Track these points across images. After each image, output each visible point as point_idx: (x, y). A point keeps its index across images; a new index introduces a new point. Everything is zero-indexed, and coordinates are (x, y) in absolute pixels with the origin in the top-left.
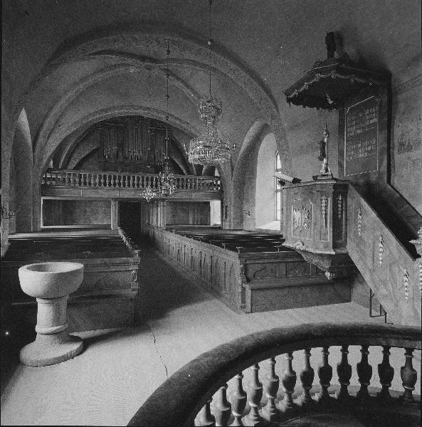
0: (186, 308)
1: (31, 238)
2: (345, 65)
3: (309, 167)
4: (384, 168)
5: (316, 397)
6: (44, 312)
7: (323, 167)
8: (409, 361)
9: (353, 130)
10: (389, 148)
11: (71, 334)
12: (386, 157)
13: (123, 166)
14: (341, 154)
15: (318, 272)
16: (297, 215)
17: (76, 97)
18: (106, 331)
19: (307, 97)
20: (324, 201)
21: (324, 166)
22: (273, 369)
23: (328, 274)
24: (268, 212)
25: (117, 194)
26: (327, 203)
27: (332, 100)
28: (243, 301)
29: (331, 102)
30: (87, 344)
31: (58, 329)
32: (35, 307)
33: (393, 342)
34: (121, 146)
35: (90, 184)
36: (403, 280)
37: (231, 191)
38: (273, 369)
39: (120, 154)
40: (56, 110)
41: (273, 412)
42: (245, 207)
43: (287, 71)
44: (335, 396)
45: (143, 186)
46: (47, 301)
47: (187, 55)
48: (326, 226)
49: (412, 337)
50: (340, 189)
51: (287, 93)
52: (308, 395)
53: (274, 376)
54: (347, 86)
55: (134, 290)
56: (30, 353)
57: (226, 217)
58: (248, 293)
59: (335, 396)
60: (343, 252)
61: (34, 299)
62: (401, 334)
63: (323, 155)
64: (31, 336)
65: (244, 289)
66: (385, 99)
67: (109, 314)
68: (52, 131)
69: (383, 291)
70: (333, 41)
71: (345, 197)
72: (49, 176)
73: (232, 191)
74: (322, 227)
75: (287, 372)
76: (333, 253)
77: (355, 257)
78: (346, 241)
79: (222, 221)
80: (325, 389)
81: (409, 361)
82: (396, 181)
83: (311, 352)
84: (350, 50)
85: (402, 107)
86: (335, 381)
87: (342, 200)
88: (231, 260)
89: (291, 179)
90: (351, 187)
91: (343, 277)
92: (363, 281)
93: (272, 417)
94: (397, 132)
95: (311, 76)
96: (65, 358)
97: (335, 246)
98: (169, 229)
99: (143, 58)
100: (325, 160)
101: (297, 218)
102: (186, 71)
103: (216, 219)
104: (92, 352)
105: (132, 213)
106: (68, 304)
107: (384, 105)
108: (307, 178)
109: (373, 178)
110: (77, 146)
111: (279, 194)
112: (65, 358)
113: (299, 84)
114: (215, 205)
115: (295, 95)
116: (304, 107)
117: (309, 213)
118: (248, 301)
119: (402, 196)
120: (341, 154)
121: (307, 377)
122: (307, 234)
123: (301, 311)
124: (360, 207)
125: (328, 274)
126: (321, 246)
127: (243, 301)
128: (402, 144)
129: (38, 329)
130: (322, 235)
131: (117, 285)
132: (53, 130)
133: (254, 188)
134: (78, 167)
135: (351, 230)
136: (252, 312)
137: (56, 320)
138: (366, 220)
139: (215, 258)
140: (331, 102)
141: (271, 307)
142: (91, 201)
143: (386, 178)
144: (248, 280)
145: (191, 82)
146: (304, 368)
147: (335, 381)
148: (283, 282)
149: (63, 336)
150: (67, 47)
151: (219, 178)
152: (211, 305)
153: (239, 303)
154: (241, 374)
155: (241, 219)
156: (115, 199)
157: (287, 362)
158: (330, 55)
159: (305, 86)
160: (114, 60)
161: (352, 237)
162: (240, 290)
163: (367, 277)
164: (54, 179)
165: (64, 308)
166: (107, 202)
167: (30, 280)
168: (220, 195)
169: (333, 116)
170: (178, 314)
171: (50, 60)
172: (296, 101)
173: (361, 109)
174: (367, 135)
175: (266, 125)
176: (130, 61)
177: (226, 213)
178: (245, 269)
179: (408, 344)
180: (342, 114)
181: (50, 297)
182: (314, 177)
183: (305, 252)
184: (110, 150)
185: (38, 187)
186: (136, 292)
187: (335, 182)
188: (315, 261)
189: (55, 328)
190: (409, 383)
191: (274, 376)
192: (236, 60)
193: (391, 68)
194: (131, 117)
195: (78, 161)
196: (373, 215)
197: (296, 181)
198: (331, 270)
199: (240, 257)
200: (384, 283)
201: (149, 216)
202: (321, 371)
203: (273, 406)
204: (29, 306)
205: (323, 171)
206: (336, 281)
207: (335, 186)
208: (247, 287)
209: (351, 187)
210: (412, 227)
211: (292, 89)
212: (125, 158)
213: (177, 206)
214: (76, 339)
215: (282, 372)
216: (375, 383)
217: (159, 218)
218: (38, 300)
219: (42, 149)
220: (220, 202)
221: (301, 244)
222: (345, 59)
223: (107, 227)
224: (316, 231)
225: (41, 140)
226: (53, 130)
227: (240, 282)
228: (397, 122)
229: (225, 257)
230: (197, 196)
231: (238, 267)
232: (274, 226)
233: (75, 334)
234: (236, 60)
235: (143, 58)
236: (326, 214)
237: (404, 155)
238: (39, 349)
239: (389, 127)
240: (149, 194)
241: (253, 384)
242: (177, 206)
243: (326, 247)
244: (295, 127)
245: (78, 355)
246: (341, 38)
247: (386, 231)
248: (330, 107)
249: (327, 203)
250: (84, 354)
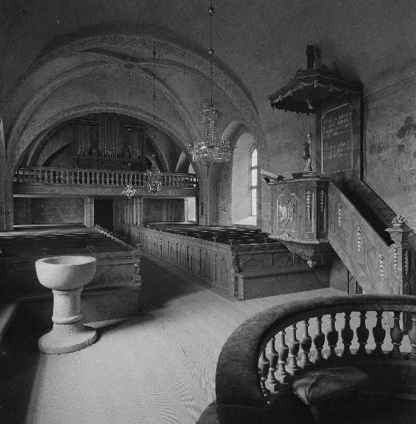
0: (184, 298)
1: (15, 236)
2: (327, 75)
3: (287, 165)
4: (358, 167)
5: (325, 357)
6: (61, 305)
7: (307, 167)
8: (397, 323)
9: (330, 132)
10: (362, 149)
11: (85, 325)
12: (359, 158)
13: (89, 163)
14: (318, 154)
15: (300, 260)
16: (283, 210)
17: (55, 93)
18: (114, 321)
19: (290, 103)
21: (308, 164)
22: (295, 334)
23: (310, 263)
24: (244, 209)
25: (94, 192)
26: (311, 198)
27: (311, 105)
28: (236, 290)
29: (310, 107)
30: (100, 333)
31: (76, 319)
32: (51, 300)
33: (386, 307)
34: (95, 144)
35: (65, 182)
36: (379, 263)
37: (206, 190)
38: (295, 334)
39: (94, 151)
40: (30, 105)
41: (294, 368)
42: (221, 203)
43: (272, 74)
44: (340, 355)
45: (124, 183)
46: (64, 293)
47: (172, 57)
48: (311, 218)
49: (399, 302)
50: (322, 186)
51: (272, 98)
52: (307, 359)
53: (295, 339)
54: (328, 94)
55: (136, 282)
56: (49, 341)
57: (202, 214)
58: (241, 282)
59: (340, 355)
60: (325, 241)
61: (49, 290)
62: (393, 301)
63: (308, 156)
64: (48, 326)
65: (236, 278)
66: (358, 106)
67: (130, 301)
68: (25, 126)
69: (362, 274)
70: (313, 53)
71: (326, 192)
72: (21, 173)
73: (170, 194)
74: (307, 219)
75: (304, 336)
76: (318, 243)
77: (335, 246)
78: (327, 232)
79: (198, 218)
80: (332, 349)
81: (397, 323)
82: (368, 179)
83: (336, 317)
84: (326, 61)
85: (372, 113)
86: (326, 347)
87: (324, 195)
88: (223, 252)
89: (277, 177)
90: (331, 183)
91: (326, 260)
92: (343, 266)
93: (295, 372)
94: (368, 135)
95: (294, 83)
96: (84, 346)
97: (318, 237)
98: (146, 224)
99: (124, 57)
100: (309, 160)
101: (283, 213)
102: (163, 71)
103: (190, 215)
104: (107, 340)
105: (106, 210)
106: (82, 297)
107: (357, 112)
108: (288, 176)
109: (348, 177)
110: (44, 143)
111: (254, 191)
112: (84, 346)
113: (284, 91)
114: (190, 203)
115: (279, 101)
116: (298, 113)
117: (295, 206)
118: (241, 289)
119: (373, 192)
120: (318, 154)
121: (333, 337)
122: (290, 225)
123: (287, 296)
124: (340, 200)
125: (310, 263)
126: (306, 236)
127: (236, 290)
128: (373, 147)
129: (54, 319)
130: (308, 228)
131: (120, 279)
132: (26, 125)
133: (229, 186)
134: (47, 164)
135: (331, 223)
136: (245, 300)
137: (73, 311)
138: (345, 211)
139: (203, 252)
140: (310, 107)
141: (262, 294)
142: (60, 199)
143: (359, 176)
144: (240, 271)
145: (169, 82)
146: (317, 332)
147: (326, 347)
148: (271, 271)
149: (79, 326)
150: (53, 45)
151: (195, 176)
152: (208, 293)
153: (233, 292)
154: (284, 331)
155: (216, 216)
156: (91, 196)
157: (293, 332)
158: (310, 66)
159: (289, 93)
160: (93, 57)
161: (333, 228)
162: (233, 280)
163: (347, 264)
164: (27, 176)
165: (79, 298)
166: (80, 201)
167: (48, 272)
168: (196, 193)
169: (311, 119)
170: (176, 303)
171: (38, 57)
172: (279, 106)
173: (337, 114)
174: (344, 137)
175: (241, 125)
176: (109, 58)
177: (202, 211)
178: (237, 260)
179: (397, 308)
180: (318, 118)
181: (66, 289)
182: (294, 175)
183: (291, 243)
184: (83, 147)
185: (10, 185)
186: (139, 284)
187: (318, 179)
188: (299, 251)
189: (72, 318)
190: (397, 341)
191: (295, 339)
192: (213, 59)
193: (363, 79)
194: (107, 114)
195: (46, 158)
196: (352, 208)
197: (280, 178)
198: (313, 259)
199: (232, 249)
200: (363, 267)
201: (123, 213)
202: (344, 332)
203: (295, 363)
204: (45, 296)
205: (307, 170)
206: (316, 268)
207: (318, 183)
208: (240, 276)
209: (331, 183)
210: (382, 218)
211: (276, 95)
212: (100, 154)
213: (152, 203)
214: (89, 329)
215: (326, 328)
216: (371, 345)
217: (135, 215)
218: (54, 292)
219: (15, 147)
220: (194, 198)
221: (287, 235)
222: (323, 70)
223: (81, 225)
224: (301, 224)
225: (13, 136)
226: (26, 125)
227: (233, 271)
228: (368, 127)
229: (215, 249)
230: (171, 193)
231: (230, 258)
232: (250, 221)
233: (89, 325)
234: (213, 59)
235: (124, 57)
236: (311, 209)
237: (375, 157)
238: (58, 338)
239: (361, 130)
240: (129, 191)
241: (292, 340)
242: (152, 203)
243: (311, 237)
244: (272, 129)
245: (95, 343)
246: (319, 52)
247: (364, 221)
248: (308, 112)
250: (98, 343)
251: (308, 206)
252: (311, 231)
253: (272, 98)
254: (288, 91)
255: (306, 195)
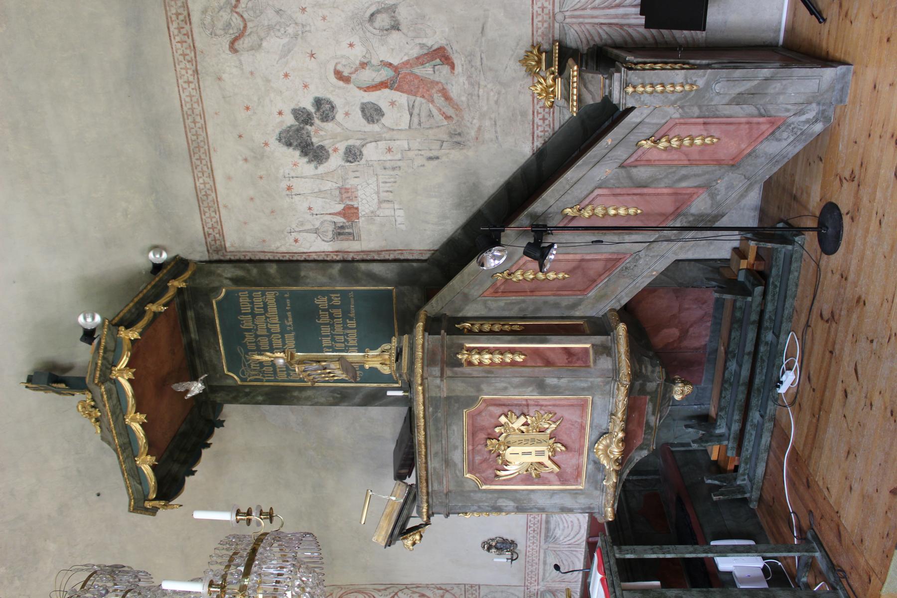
20: (475, 358)
26: (480, 351)
51: (139, 506)
117: (509, 408)
126: (605, 363)
221: (604, 442)
243: (605, 350)
249: (480, 351)
251: (508, 358)
252: (586, 349)
253: (139, 506)
254: (128, 428)
255: (470, 363)
